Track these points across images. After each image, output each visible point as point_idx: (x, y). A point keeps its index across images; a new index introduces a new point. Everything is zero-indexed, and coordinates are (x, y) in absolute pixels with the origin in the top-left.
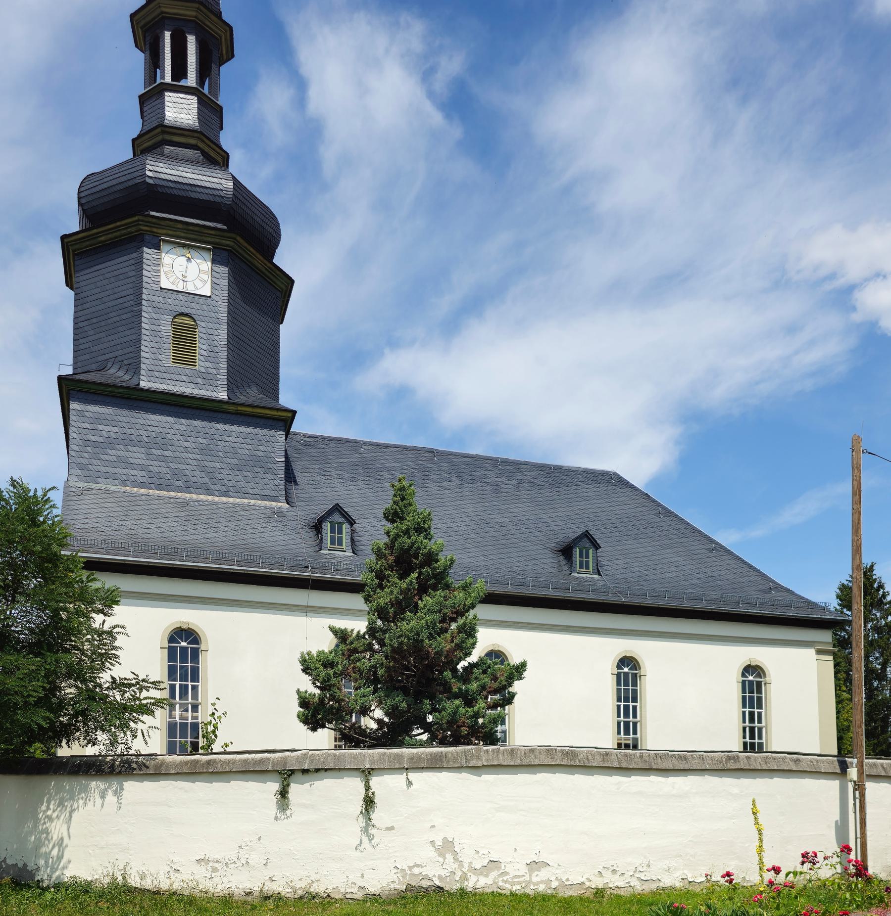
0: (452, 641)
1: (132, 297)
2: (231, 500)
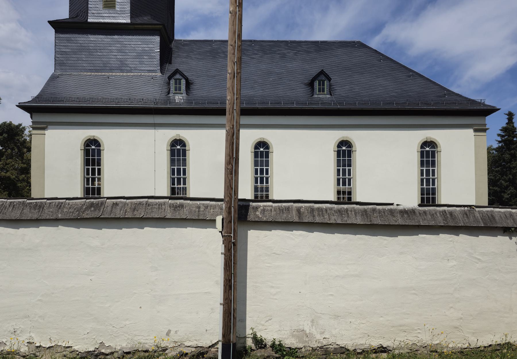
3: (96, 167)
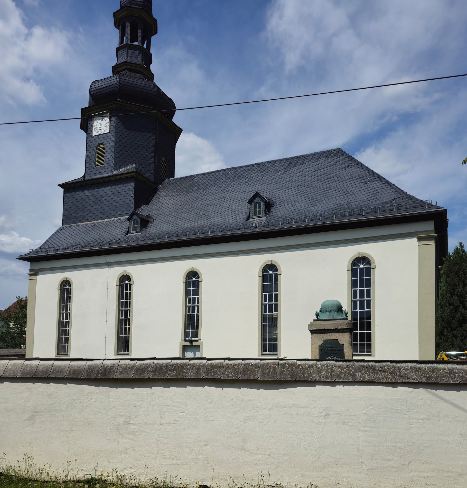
3: (365, 289)
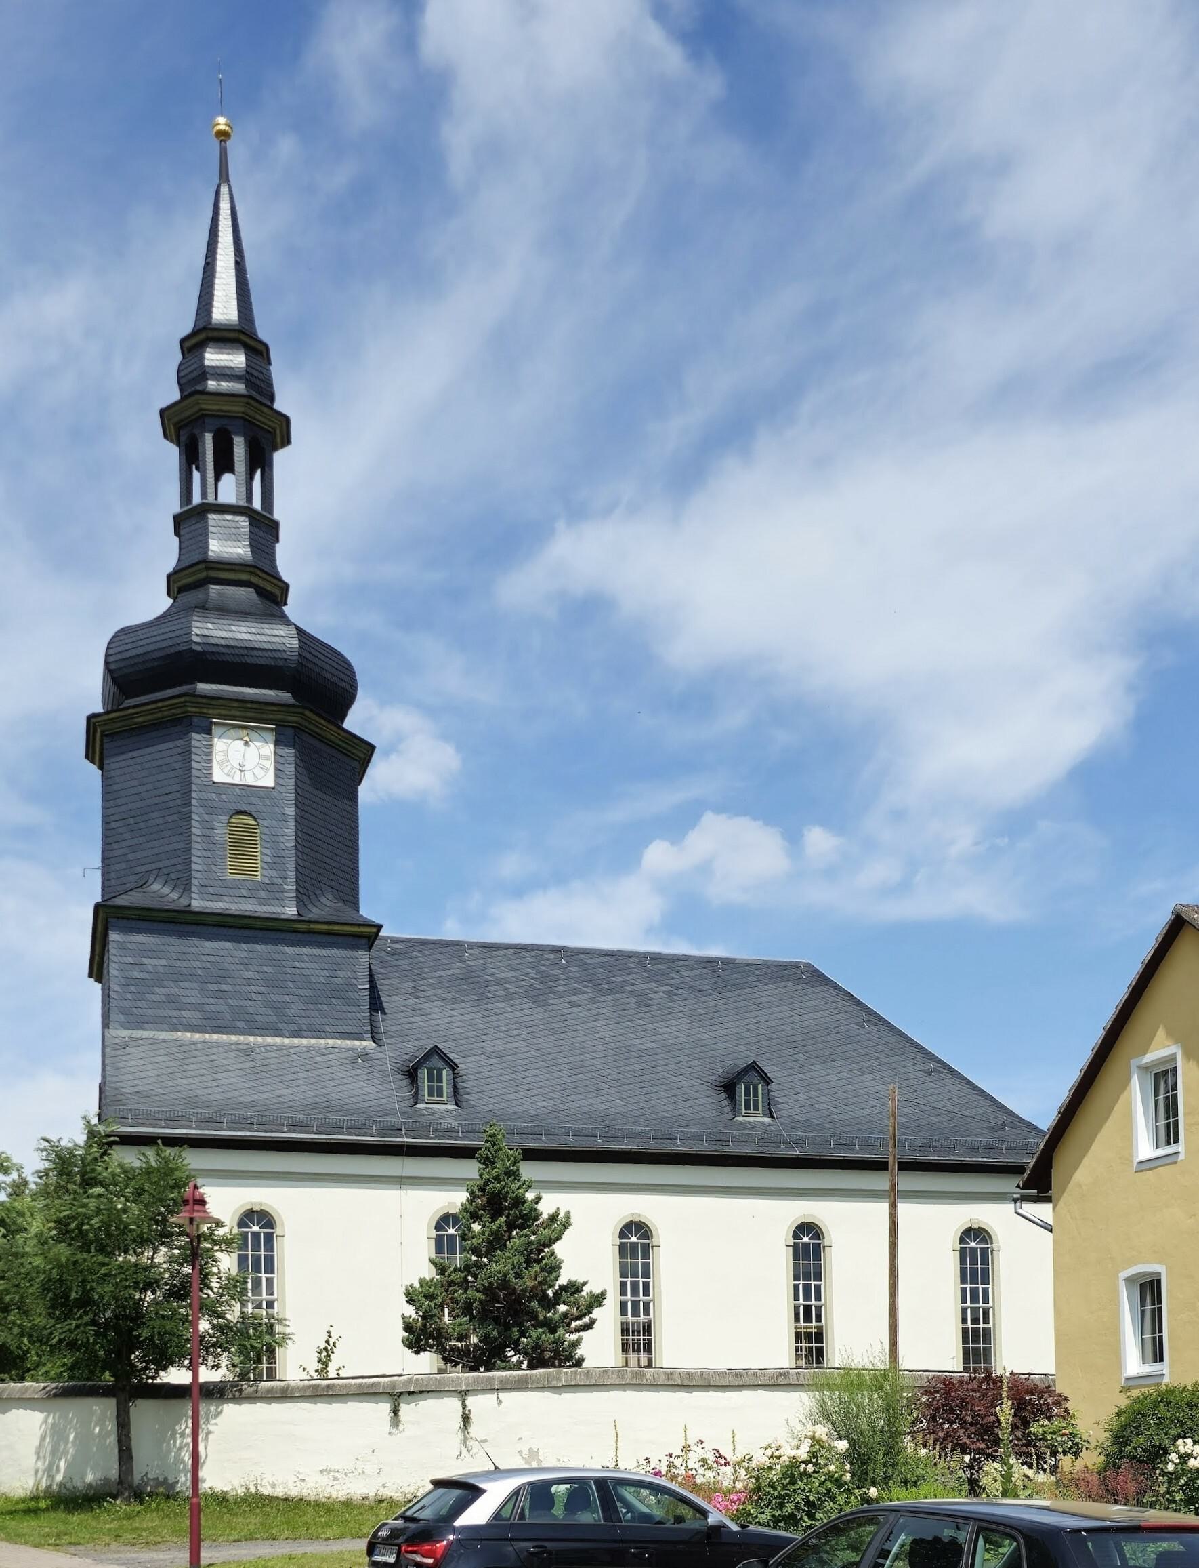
0: (536, 1279)
1: (178, 795)
2: (304, 1041)
3: (980, 1286)
